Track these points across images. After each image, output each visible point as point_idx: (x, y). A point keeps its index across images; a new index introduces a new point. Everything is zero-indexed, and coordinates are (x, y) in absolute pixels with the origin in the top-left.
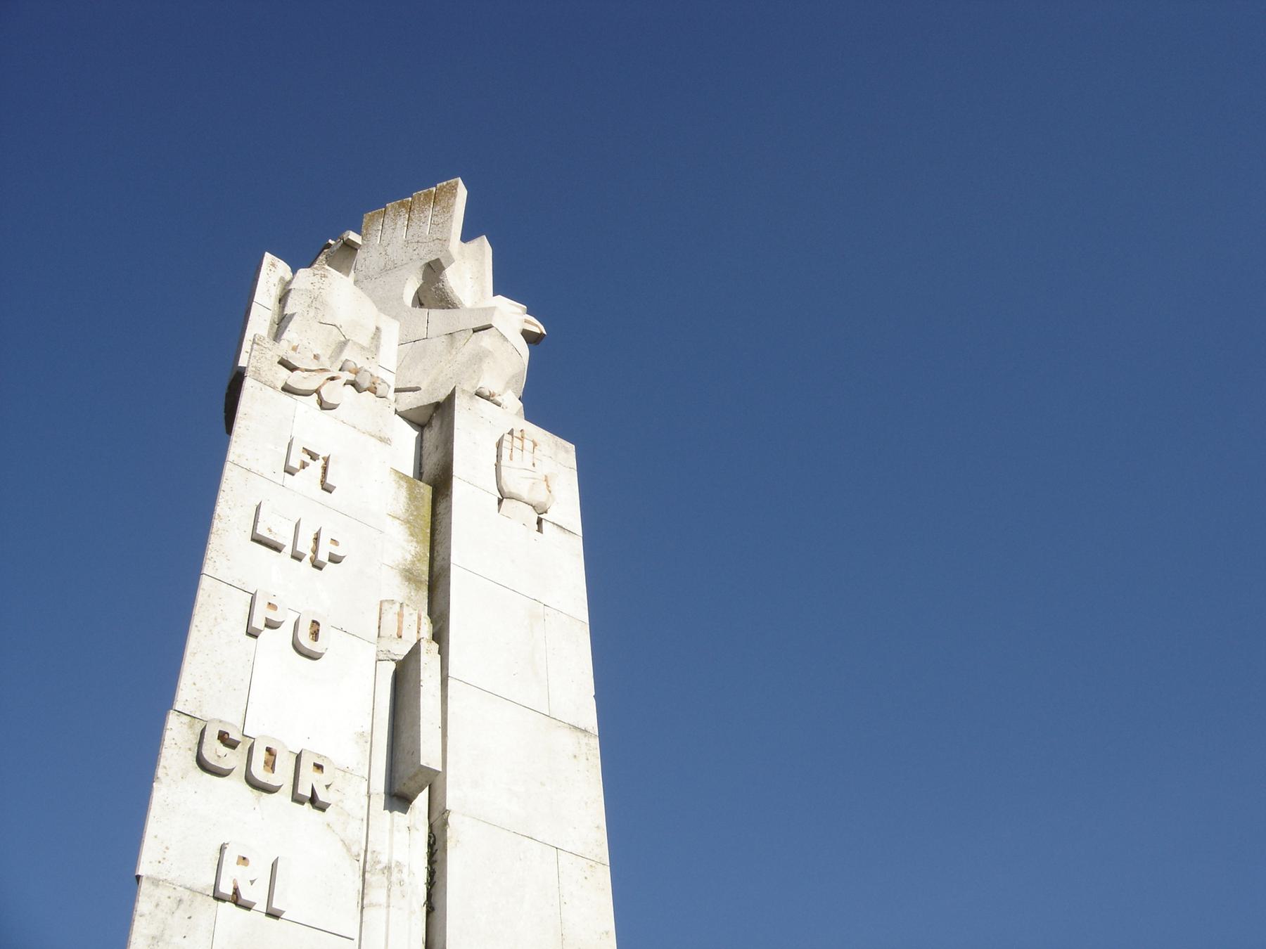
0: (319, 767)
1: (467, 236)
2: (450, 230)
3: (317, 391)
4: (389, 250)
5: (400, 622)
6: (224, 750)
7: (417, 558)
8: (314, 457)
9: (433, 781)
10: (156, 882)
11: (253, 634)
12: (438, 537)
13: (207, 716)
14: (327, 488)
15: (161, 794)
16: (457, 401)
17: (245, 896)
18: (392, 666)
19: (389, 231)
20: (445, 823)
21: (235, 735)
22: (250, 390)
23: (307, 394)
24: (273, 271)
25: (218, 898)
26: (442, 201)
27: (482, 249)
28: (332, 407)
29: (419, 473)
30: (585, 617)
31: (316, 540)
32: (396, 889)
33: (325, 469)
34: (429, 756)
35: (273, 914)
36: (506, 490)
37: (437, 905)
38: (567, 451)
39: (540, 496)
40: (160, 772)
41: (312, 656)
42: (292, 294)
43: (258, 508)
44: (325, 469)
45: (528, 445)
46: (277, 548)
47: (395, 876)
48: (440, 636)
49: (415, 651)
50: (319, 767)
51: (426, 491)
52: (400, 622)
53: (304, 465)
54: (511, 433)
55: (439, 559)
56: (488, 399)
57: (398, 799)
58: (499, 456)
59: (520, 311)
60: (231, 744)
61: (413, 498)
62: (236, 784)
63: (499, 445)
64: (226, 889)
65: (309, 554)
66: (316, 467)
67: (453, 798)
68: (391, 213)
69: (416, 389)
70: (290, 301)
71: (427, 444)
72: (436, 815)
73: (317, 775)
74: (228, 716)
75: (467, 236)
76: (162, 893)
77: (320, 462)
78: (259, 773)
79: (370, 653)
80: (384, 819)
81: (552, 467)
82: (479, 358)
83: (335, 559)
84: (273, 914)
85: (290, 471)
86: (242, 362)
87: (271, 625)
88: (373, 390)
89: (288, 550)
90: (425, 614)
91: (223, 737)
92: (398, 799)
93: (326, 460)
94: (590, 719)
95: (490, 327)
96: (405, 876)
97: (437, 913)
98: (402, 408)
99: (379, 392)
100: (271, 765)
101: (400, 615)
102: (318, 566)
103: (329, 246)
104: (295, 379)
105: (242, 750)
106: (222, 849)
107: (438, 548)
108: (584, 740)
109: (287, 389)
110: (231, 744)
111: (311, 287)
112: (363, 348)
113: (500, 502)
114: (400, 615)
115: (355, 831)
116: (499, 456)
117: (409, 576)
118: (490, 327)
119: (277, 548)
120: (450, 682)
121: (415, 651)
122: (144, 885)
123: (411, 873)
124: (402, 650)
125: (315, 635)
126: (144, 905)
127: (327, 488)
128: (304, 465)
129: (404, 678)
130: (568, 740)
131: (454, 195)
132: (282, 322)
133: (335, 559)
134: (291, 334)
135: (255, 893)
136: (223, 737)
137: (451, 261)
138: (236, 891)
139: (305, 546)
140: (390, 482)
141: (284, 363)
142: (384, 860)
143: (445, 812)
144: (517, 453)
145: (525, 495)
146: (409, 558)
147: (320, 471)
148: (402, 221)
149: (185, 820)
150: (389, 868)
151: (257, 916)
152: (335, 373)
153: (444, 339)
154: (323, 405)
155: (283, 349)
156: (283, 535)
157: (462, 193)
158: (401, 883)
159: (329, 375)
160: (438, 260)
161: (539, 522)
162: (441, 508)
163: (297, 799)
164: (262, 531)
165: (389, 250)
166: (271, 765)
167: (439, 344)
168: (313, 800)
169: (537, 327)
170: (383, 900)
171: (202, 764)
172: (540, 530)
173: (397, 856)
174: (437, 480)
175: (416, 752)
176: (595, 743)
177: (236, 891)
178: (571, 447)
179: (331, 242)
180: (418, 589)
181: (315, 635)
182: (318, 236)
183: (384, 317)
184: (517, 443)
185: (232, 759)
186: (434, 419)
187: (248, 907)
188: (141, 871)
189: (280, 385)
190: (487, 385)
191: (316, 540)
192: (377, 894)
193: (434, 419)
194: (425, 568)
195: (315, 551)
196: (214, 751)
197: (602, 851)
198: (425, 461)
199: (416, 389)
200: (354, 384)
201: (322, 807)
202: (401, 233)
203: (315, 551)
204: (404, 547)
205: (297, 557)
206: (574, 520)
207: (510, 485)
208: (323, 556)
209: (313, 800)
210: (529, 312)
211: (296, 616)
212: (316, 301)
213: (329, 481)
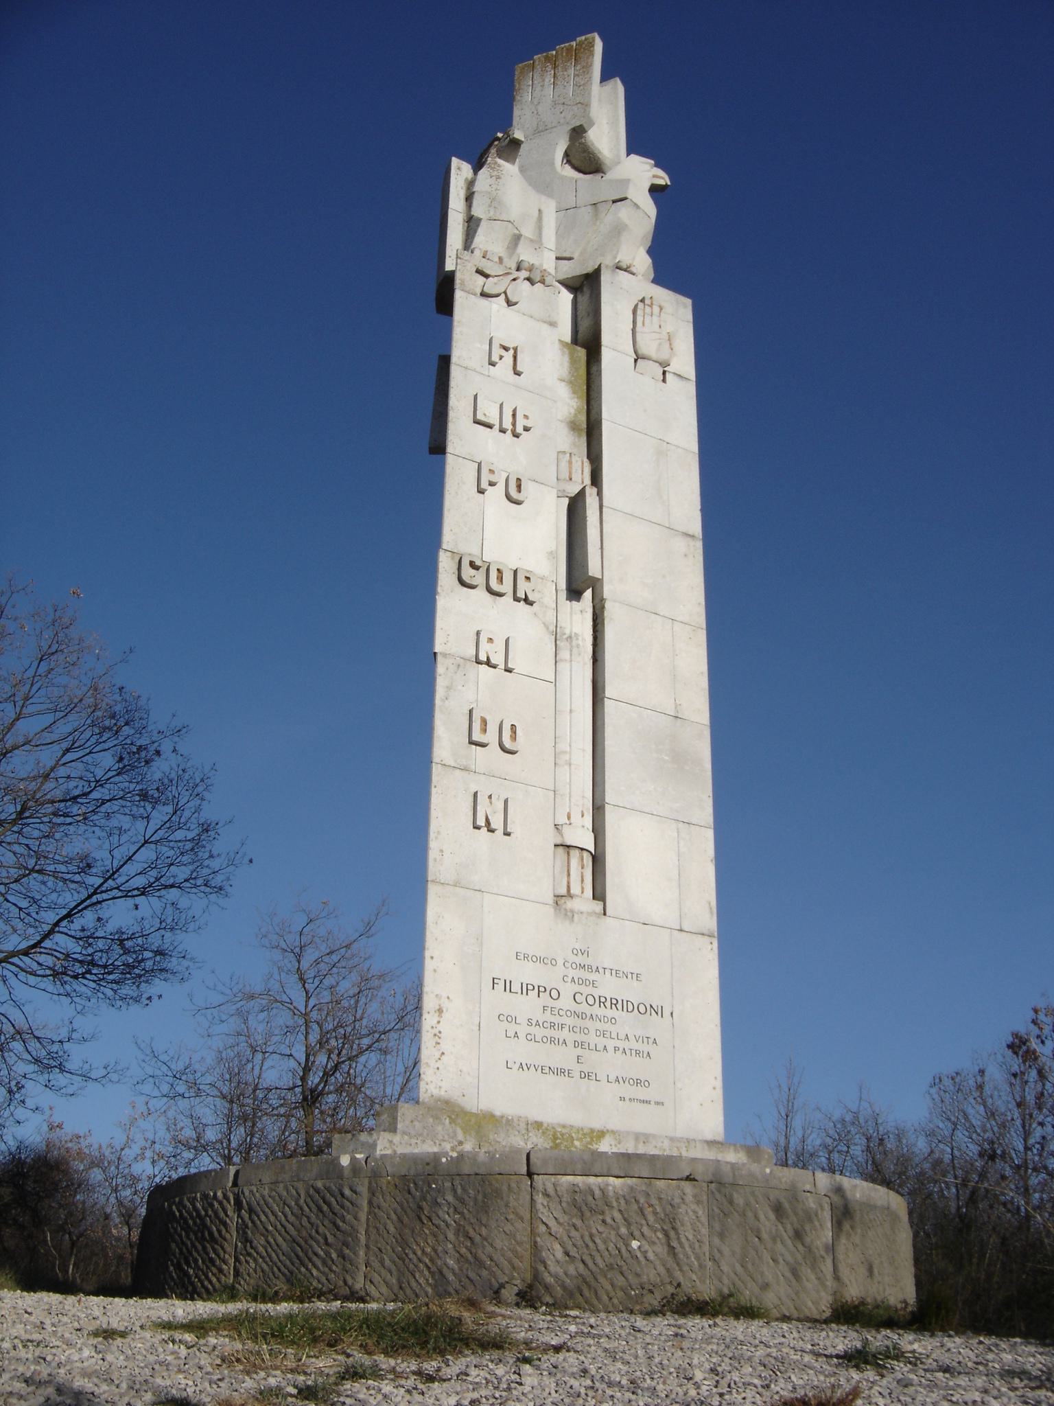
0: (528, 578)
1: (606, 77)
2: (589, 94)
3: (505, 293)
4: (540, 108)
5: (570, 468)
6: (473, 572)
7: (578, 411)
8: (506, 349)
9: (596, 584)
10: (445, 655)
11: (481, 491)
12: (593, 394)
13: (462, 551)
14: (518, 374)
15: (442, 602)
16: (603, 278)
17: (493, 661)
18: (566, 501)
19: (538, 89)
20: (603, 607)
21: (478, 563)
22: (459, 295)
23: (497, 296)
24: (460, 171)
25: (478, 662)
26: (580, 56)
27: (617, 88)
28: (516, 304)
29: (575, 340)
30: (695, 447)
31: (514, 415)
32: (575, 650)
33: (515, 357)
34: (594, 569)
35: (508, 670)
36: (640, 352)
37: (599, 658)
38: (685, 307)
39: (664, 356)
40: (439, 589)
41: (518, 503)
42: (476, 196)
43: (476, 397)
44: (515, 357)
45: (656, 309)
46: (490, 426)
47: (574, 643)
48: (596, 479)
49: (582, 493)
50: (528, 578)
51: (582, 353)
52: (570, 468)
53: (501, 357)
54: (643, 300)
55: (593, 412)
56: (625, 270)
57: (574, 593)
58: (634, 322)
59: (647, 167)
60: (477, 568)
61: (573, 361)
62: (481, 593)
63: (635, 312)
64: (483, 658)
65: (510, 427)
66: (509, 356)
67: (607, 591)
68: (538, 68)
69: (570, 259)
70: (475, 203)
71: (580, 307)
72: (597, 601)
73: (527, 584)
74: (470, 549)
75: (605, 78)
76: (449, 662)
77: (512, 352)
78: (494, 585)
79: (554, 493)
80: (567, 606)
81: (674, 322)
82: (618, 230)
83: (526, 429)
84: (508, 670)
85: (493, 364)
86: (449, 266)
87: (492, 484)
88: (543, 282)
89: (497, 427)
90: (585, 460)
91: (473, 565)
92: (574, 593)
93: (515, 349)
94: (696, 527)
95: (625, 199)
96: (580, 642)
97: (599, 663)
98: (562, 277)
99: (547, 282)
100: (500, 579)
101: (570, 462)
102: (516, 436)
103: (498, 139)
104: (491, 286)
105: (483, 571)
106: (478, 633)
107: (592, 402)
108: (692, 543)
109: (484, 295)
110: (477, 568)
111: (489, 189)
112: (532, 241)
113: (636, 361)
114: (570, 462)
115: (551, 616)
116: (634, 322)
117: (573, 426)
118: (625, 199)
119: (490, 426)
120: (609, 705)
121: (582, 493)
122: (439, 658)
123: (584, 640)
124: (574, 490)
125: (519, 487)
126: (440, 669)
127: (518, 374)
128: (501, 357)
129: (575, 508)
130: (680, 545)
131: (592, 54)
132: (472, 224)
133: (526, 429)
134: (480, 240)
135: (498, 659)
136: (473, 565)
137: (592, 124)
138: (488, 658)
139: (507, 424)
140: (557, 345)
141: (479, 272)
142: (568, 632)
143: (602, 600)
144: (648, 319)
145: (653, 354)
146: (573, 411)
147: (512, 359)
148: (549, 79)
149: (458, 616)
150: (570, 637)
151: (500, 671)
152: (516, 274)
153: (590, 209)
154: (510, 303)
155: (476, 260)
156: (493, 418)
157: (599, 46)
158: (578, 646)
159: (512, 277)
160: (581, 126)
161: (664, 373)
162: (594, 369)
163: (517, 599)
164: (480, 417)
165: (540, 108)
166: (500, 579)
167: (585, 213)
168: (526, 600)
169: (663, 179)
170: (568, 657)
171: (462, 582)
172: (664, 381)
173: (575, 630)
174: (588, 341)
175: (585, 565)
176: (699, 544)
177: (488, 658)
178: (688, 302)
179: (500, 135)
180: (580, 436)
181: (519, 487)
182: (489, 138)
183: (544, 198)
184: (648, 309)
185: (479, 578)
186: (586, 287)
187: (494, 667)
188: (438, 648)
189: (479, 291)
190: (624, 257)
191: (514, 415)
192: (564, 654)
193: (586, 287)
194: (584, 418)
195: (514, 424)
196: (468, 573)
197: (701, 620)
198: (580, 322)
199: (570, 259)
200: (528, 279)
201: (531, 604)
202: (549, 90)
203: (514, 424)
204: (568, 403)
205: (503, 431)
206: (690, 371)
207: (644, 349)
208: (519, 429)
209: (526, 600)
210: (657, 165)
211: (504, 475)
212: (494, 202)
213: (519, 368)
